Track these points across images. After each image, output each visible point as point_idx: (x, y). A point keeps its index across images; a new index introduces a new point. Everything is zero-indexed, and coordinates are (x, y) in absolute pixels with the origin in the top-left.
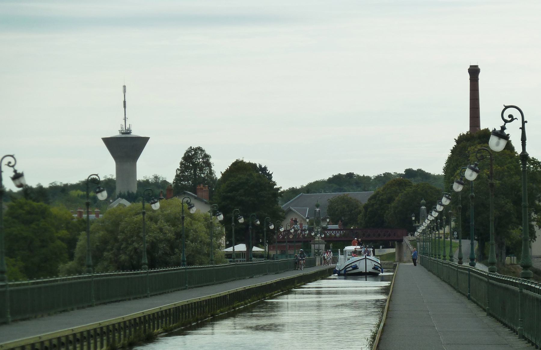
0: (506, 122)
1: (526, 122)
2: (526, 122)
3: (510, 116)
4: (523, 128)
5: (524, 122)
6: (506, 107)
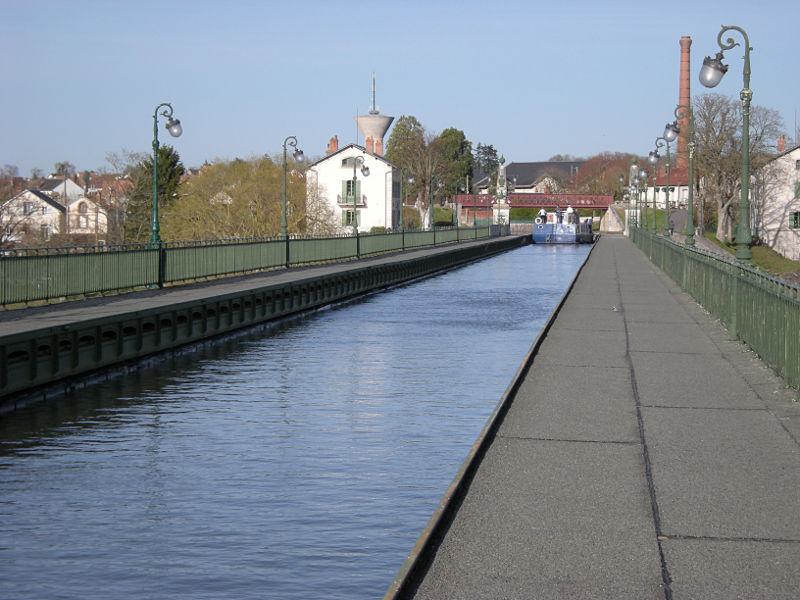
0: (724, 48)
1: (751, 49)
2: (751, 49)
3: (730, 40)
4: (747, 58)
5: (748, 49)
6: (726, 29)
